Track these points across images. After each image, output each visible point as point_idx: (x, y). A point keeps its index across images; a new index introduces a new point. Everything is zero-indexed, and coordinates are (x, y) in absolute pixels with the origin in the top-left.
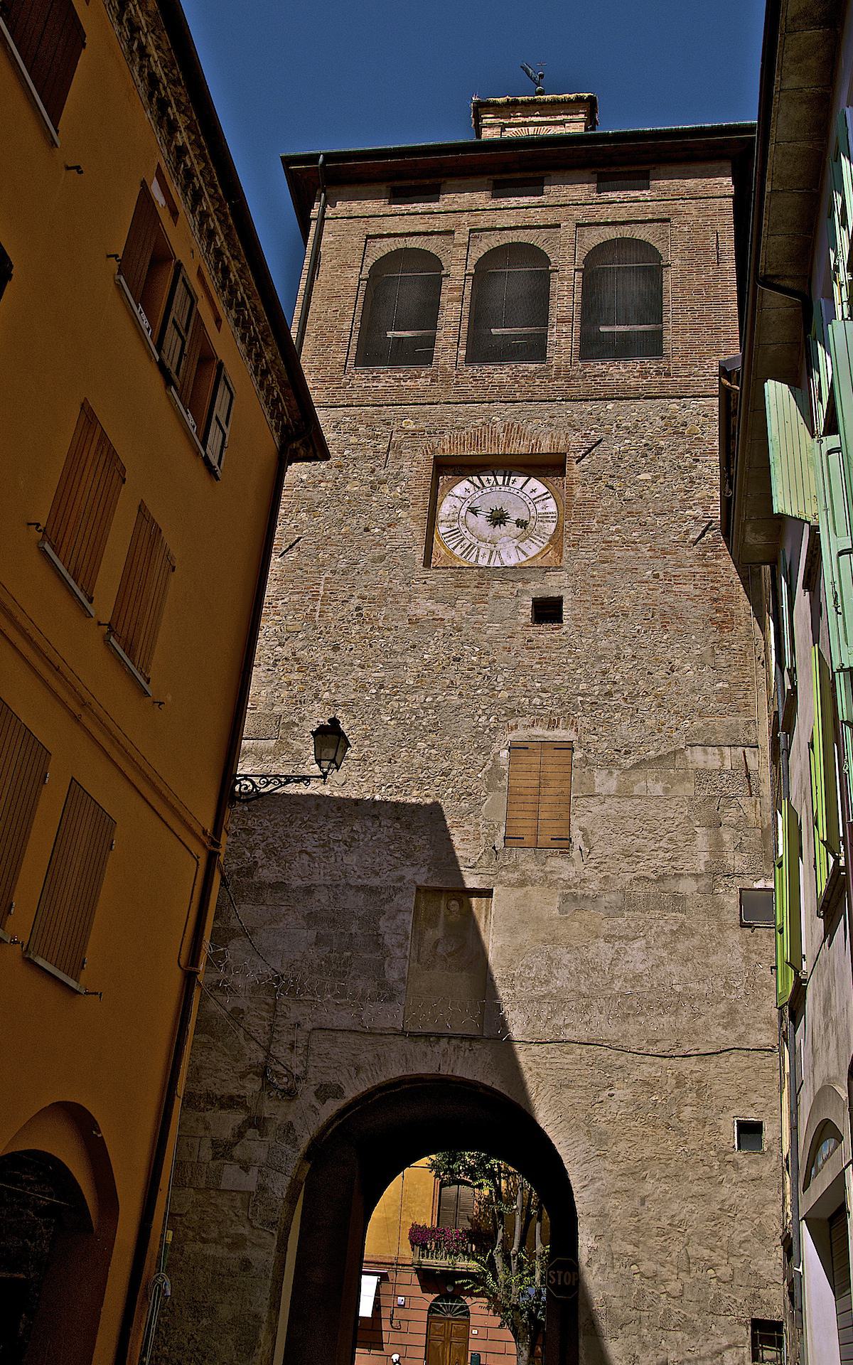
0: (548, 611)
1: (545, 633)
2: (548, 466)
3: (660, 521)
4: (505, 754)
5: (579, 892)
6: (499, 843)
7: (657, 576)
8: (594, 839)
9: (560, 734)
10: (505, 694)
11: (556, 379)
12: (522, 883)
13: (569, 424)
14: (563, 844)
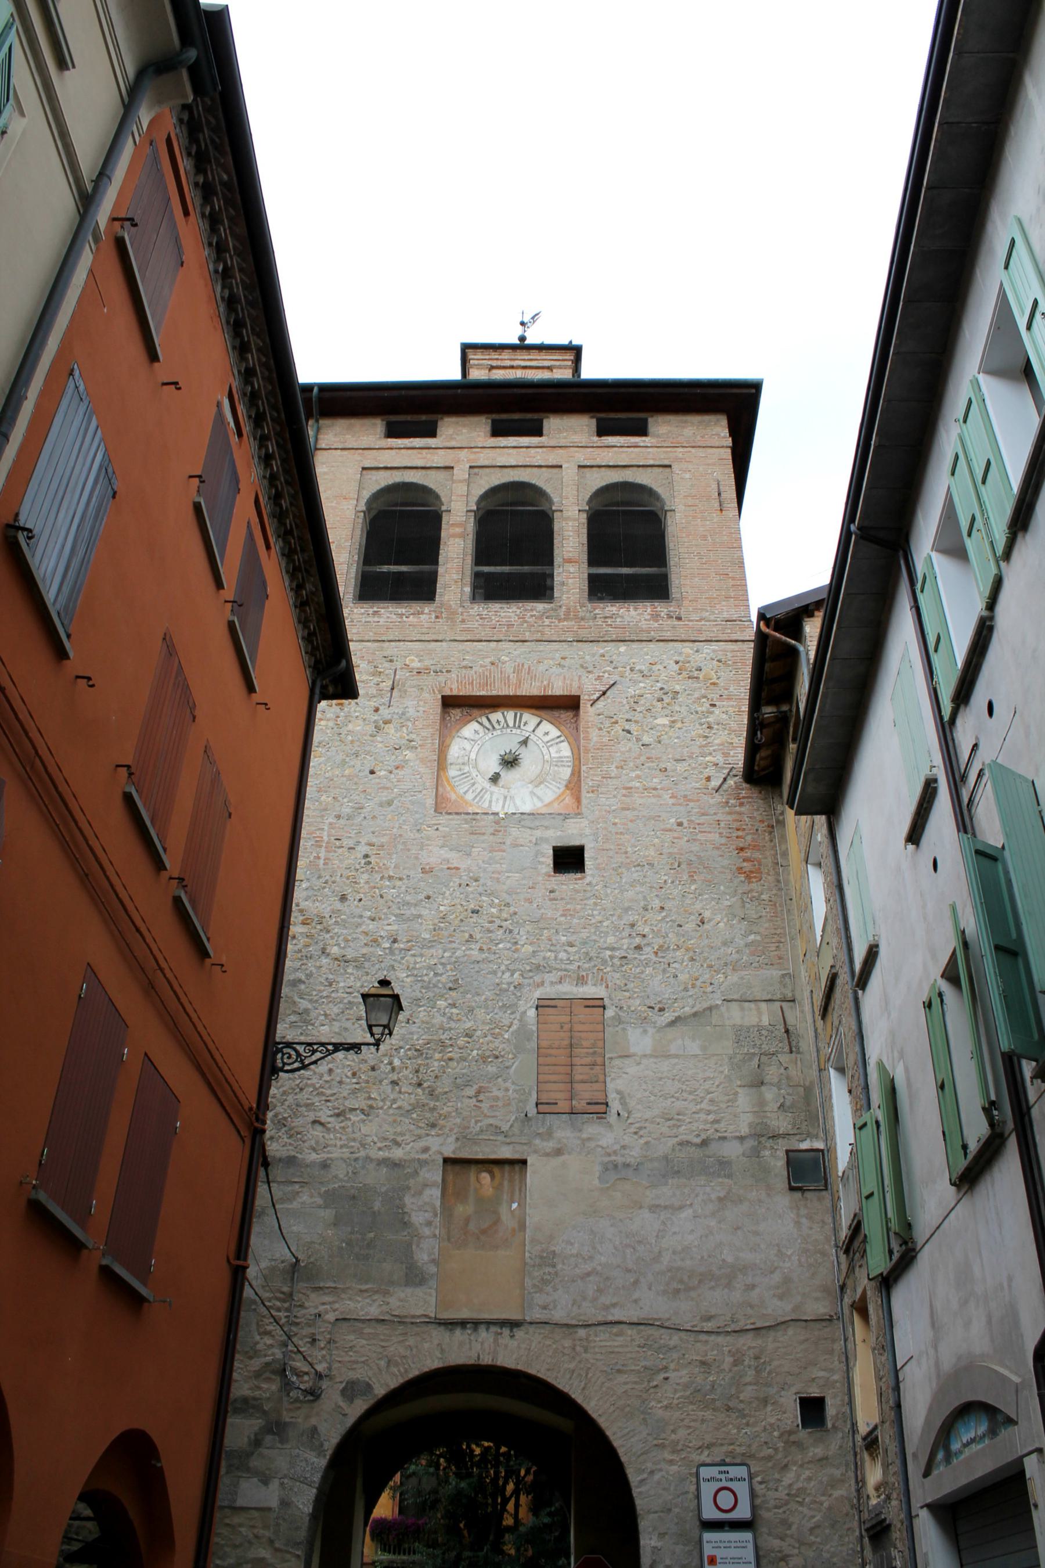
3: (680, 767)
5: (619, 1160)
9: (590, 990)
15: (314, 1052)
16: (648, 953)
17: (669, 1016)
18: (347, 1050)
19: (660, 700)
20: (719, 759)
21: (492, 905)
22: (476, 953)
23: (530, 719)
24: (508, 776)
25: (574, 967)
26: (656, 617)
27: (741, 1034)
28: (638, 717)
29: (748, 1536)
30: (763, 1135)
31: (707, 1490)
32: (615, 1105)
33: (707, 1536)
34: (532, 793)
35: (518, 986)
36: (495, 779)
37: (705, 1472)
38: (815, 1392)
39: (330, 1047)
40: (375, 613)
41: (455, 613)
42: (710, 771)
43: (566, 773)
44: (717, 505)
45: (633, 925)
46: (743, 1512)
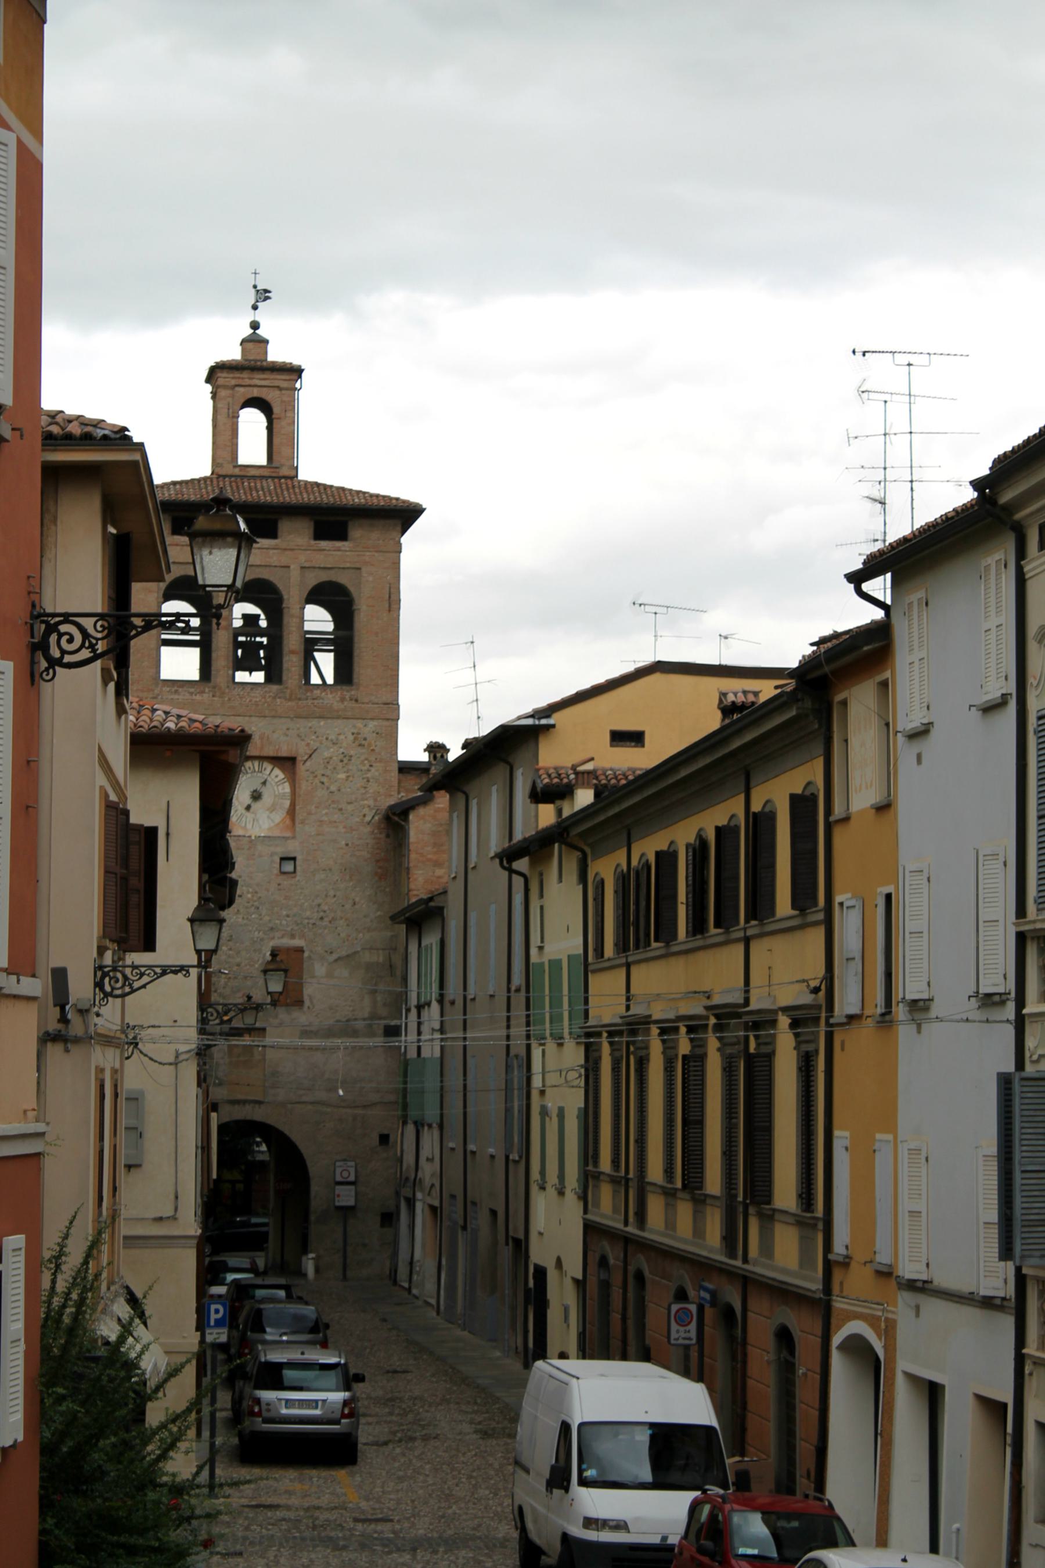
3: (350, 808)
5: (308, 1028)
9: (297, 942)
11: (290, 699)
13: (299, 736)
14: (299, 1003)
15: (142, 975)
16: (325, 922)
17: (335, 956)
18: (175, 972)
19: (342, 761)
20: (371, 802)
21: (248, 892)
22: (240, 920)
23: (268, 766)
24: (256, 806)
25: (289, 929)
26: (342, 700)
27: (369, 967)
28: (328, 773)
29: (353, 1187)
30: (374, 1016)
31: (338, 1171)
32: (307, 1003)
33: (337, 1187)
34: (269, 817)
35: (262, 940)
36: (248, 808)
37: (338, 1164)
38: (386, 1132)
39: (158, 970)
40: (176, 692)
41: (224, 693)
42: (366, 811)
43: (287, 803)
44: (387, 605)
45: (319, 905)
46: (352, 1178)
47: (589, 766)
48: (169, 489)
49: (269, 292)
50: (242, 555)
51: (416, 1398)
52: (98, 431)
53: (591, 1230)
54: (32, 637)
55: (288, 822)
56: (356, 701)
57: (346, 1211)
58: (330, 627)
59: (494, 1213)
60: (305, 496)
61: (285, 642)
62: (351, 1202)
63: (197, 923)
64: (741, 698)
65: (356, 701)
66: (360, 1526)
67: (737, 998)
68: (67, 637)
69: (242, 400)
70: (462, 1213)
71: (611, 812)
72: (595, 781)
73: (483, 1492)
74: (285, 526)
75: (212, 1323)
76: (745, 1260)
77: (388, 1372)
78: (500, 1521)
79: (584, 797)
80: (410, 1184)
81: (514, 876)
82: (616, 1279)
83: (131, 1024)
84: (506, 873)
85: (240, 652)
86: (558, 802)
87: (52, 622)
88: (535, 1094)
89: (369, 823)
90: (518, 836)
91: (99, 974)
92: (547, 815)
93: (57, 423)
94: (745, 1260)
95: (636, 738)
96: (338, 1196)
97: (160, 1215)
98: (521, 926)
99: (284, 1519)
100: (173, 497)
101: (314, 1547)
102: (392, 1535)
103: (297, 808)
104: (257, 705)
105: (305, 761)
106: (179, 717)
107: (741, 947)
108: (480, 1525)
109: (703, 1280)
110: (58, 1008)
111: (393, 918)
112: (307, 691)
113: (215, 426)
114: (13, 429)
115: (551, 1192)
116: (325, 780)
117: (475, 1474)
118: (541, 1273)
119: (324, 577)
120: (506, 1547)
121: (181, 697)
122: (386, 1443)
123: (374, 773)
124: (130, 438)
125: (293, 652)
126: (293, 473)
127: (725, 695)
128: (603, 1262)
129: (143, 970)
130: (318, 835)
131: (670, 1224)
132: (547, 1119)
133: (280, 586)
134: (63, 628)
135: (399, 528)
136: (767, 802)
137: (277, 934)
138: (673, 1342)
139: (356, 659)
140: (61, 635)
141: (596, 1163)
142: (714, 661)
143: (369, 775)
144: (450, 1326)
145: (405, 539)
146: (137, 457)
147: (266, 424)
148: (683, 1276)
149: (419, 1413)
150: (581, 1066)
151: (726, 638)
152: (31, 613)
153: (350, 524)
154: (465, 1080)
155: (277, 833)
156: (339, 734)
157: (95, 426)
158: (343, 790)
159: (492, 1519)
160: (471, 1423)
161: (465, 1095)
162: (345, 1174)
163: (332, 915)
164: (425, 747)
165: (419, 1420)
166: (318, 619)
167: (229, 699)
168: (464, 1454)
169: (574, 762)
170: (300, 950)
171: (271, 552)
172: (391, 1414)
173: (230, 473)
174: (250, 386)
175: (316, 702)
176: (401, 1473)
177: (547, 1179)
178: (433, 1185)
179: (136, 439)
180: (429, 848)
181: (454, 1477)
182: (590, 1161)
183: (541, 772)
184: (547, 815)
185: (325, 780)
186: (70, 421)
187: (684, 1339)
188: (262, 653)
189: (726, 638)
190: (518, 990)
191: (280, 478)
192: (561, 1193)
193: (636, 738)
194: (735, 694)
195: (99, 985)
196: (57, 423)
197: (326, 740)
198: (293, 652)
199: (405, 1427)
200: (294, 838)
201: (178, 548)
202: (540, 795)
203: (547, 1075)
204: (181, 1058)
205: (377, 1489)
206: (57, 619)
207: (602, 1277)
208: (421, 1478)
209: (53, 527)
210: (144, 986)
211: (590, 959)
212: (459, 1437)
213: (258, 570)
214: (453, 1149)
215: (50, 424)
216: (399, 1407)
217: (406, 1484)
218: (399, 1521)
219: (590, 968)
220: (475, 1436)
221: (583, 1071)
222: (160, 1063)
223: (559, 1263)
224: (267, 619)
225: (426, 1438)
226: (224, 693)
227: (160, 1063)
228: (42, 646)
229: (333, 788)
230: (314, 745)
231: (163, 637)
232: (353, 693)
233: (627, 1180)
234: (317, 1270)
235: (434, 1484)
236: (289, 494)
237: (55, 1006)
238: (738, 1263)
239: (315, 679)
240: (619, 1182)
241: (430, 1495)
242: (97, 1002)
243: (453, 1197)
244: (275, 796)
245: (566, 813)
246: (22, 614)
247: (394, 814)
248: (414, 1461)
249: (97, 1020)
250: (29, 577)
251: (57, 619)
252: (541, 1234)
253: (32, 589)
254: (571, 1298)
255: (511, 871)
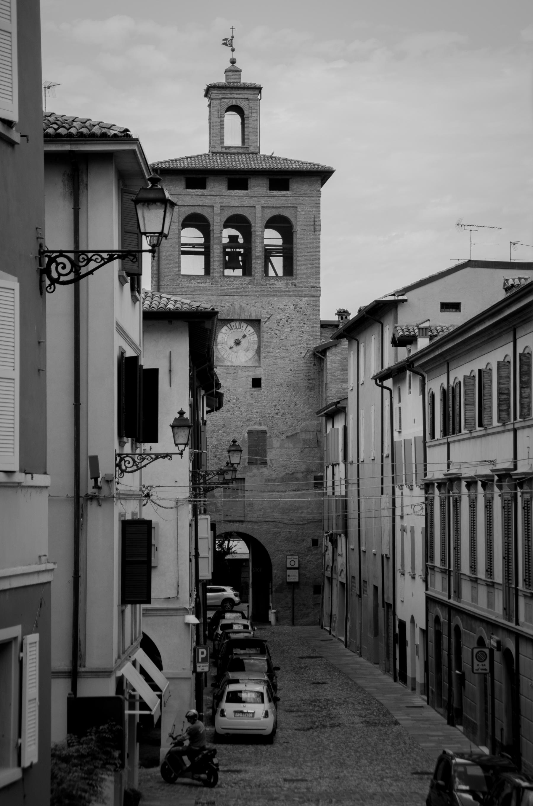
0: (257, 383)
1: (256, 391)
2: (255, 323)
3: (293, 348)
4: (246, 435)
5: (270, 478)
6: (246, 464)
7: (291, 370)
8: (273, 462)
9: (263, 428)
10: (246, 414)
11: (256, 286)
12: (254, 476)
13: (262, 307)
14: (264, 463)
15: (144, 459)
16: (279, 416)
18: (163, 457)
19: (287, 321)
20: (305, 345)
21: (234, 399)
22: (229, 415)
23: (244, 325)
25: (258, 420)
26: (287, 285)
27: (305, 441)
28: (280, 328)
29: (297, 571)
30: (308, 471)
32: (269, 463)
33: (288, 571)
37: (288, 557)
38: (316, 538)
43: (256, 346)
46: (297, 565)
47: (426, 325)
48: (172, 162)
49: (223, 44)
50: (168, 215)
51: (329, 700)
52: (111, 131)
53: (429, 600)
54: (40, 265)
55: (256, 357)
56: (295, 285)
57: (294, 585)
58: (280, 242)
59: (376, 588)
60: (264, 164)
61: (253, 252)
62: (297, 580)
63: (176, 428)
64: (517, 282)
65: (295, 285)
66: (287, 785)
67: (509, 465)
68: (61, 266)
69: (226, 107)
70: (358, 587)
71: (437, 353)
72: (430, 333)
73: (364, 761)
74: (252, 183)
75: (200, 660)
76: (517, 623)
77: (314, 683)
78: (371, 782)
79: (423, 343)
80: (329, 569)
81: (385, 390)
82: (445, 631)
83: (146, 485)
84: (380, 388)
85: (227, 258)
86: (409, 346)
87: (53, 256)
88: (398, 519)
89: (304, 357)
90: (386, 366)
91: (118, 459)
92: (403, 353)
93: (86, 127)
94: (517, 623)
95: (456, 307)
96: (289, 576)
97: (168, 596)
98: (390, 420)
99: (242, 780)
100: (186, 166)
101: (259, 798)
102: (305, 790)
103: (262, 349)
104: (237, 289)
105: (266, 322)
106: (176, 301)
107: (512, 434)
108: (359, 784)
109: (493, 634)
110: (93, 480)
111: (318, 413)
112: (266, 280)
113: (210, 123)
114: (22, 136)
115: (408, 577)
116: (277, 332)
117: (359, 750)
118: (402, 624)
119: (275, 212)
120: (374, 799)
121: (193, 285)
122: (308, 729)
123: (306, 328)
124: (129, 136)
125: (258, 257)
126: (257, 151)
127: (507, 280)
128: (437, 620)
129: (144, 456)
130: (274, 365)
131: (474, 599)
132: (405, 533)
133: (250, 218)
134: (59, 260)
135: (319, 182)
136: (526, 347)
137: (252, 423)
138: (475, 671)
139: (295, 261)
140: (58, 264)
141: (432, 560)
142: (506, 259)
143: (303, 329)
144: (354, 654)
145: (322, 190)
146: (135, 147)
147: (241, 121)
148: (482, 631)
149: (329, 710)
150: (423, 503)
151: (514, 244)
152: (39, 251)
153: (290, 180)
154: (359, 511)
155: (250, 364)
156: (286, 305)
157: (109, 128)
158: (288, 338)
159: (367, 780)
160: (360, 716)
161: (359, 520)
162: (293, 563)
163: (283, 411)
164: (336, 312)
165: (329, 715)
166: (272, 238)
167: (221, 286)
168: (354, 736)
169: (418, 323)
170: (264, 432)
171: (244, 198)
172: (313, 710)
173: (220, 151)
174: (231, 98)
175: (271, 286)
176: (315, 749)
177: (405, 569)
178: (342, 570)
179: (134, 137)
180: (339, 372)
181: (347, 752)
182: (429, 559)
183: (398, 328)
184: (403, 353)
185: (277, 332)
186: (94, 126)
187: (482, 669)
188: (240, 258)
189: (514, 244)
190: (387, 457)
191: (249, 153)
192: (413, 578)
193: (456, 307)
194: (514, 280)
195: (118, 465)
196: (86, 127)
197: (278, 308)
198: (258, 257)
199: (321, 719)
200: (260, 367)
201: (190, 197)
202: (398, 342)
203: (404, 508)
204: (179, 504)
205: (301, 759)
206: (55, 255)
207: (437, 629)
208: (328, 752)
209: (85, 191)
210: (145, 466)
211: (427, 440)
212: (351, 725)
213: (236, 209)
214: (353, 549)
215: (83, 127)
216: (318, 706)
217: (318, 755)
218: (311, 781)
219: (427, 444)
220: (361, 725)
221: (424, 506)
222: (165, 508)
223: (413, 619)
224: (244, 238)
225: (332, 726)
226: (217, 282)
227: (165, 508)
228: (47, 271)
229: (282, 337)
230: (271, 312)
231: (182, 249)
232: (293, 281)
233: (450, 571)
234: (277, 620)
235: (335, 756)
236: (254, 163)
237: (91, 479)
238: (513, 625)
239: (271, 273)
240: (447, 572)
241: (331, 763)
242: (117, 476)
243: (353, 577)
244: (249, 342)
245: (413, 352)
246: (34, 252)
247: (318, 352)
248: (324, 741)
249: (119, 486)
250: (37, 228)
251: (55, 255)
252: (402, 601)
253: (39, 236)
254: (418, 640)
255: (383, 387)
